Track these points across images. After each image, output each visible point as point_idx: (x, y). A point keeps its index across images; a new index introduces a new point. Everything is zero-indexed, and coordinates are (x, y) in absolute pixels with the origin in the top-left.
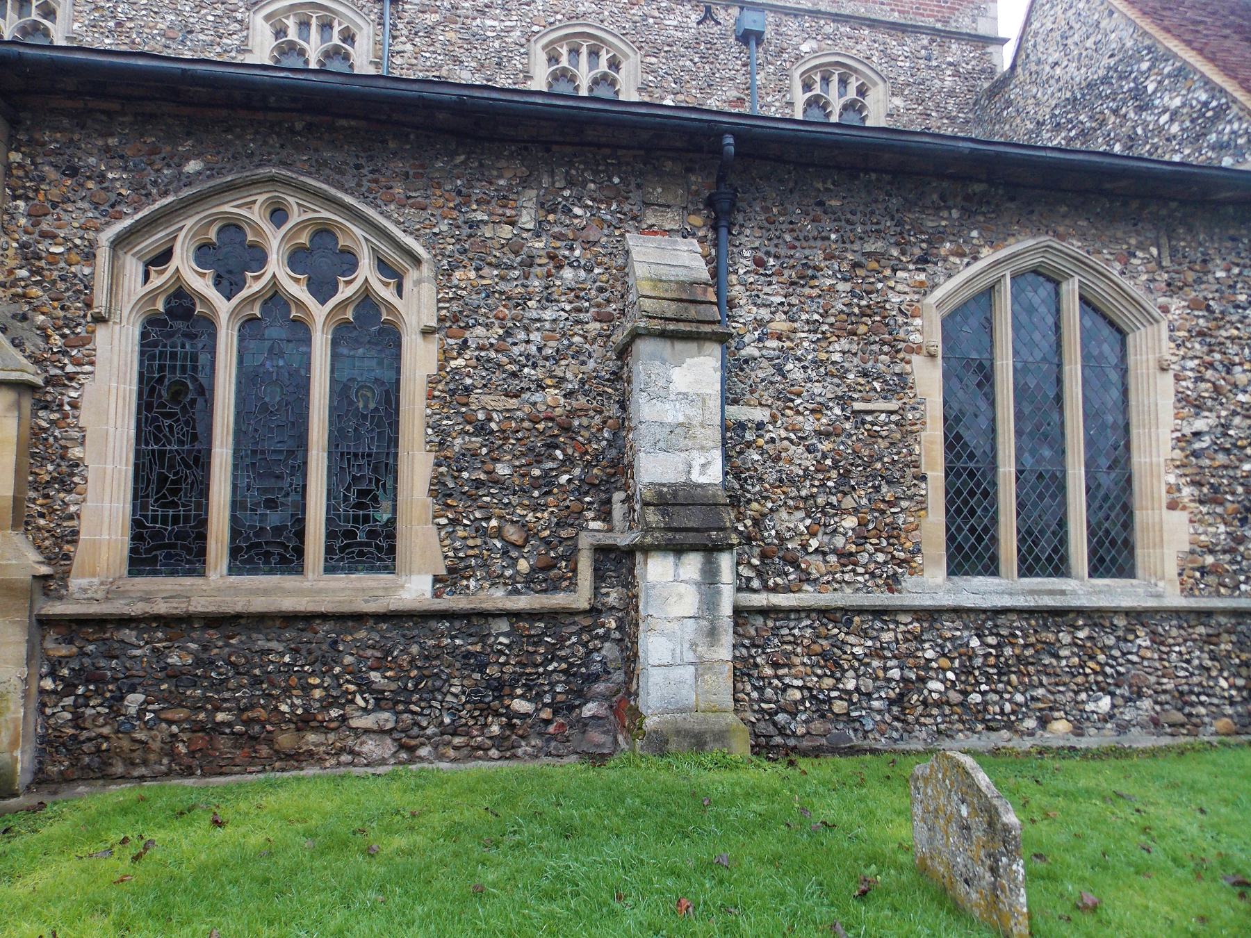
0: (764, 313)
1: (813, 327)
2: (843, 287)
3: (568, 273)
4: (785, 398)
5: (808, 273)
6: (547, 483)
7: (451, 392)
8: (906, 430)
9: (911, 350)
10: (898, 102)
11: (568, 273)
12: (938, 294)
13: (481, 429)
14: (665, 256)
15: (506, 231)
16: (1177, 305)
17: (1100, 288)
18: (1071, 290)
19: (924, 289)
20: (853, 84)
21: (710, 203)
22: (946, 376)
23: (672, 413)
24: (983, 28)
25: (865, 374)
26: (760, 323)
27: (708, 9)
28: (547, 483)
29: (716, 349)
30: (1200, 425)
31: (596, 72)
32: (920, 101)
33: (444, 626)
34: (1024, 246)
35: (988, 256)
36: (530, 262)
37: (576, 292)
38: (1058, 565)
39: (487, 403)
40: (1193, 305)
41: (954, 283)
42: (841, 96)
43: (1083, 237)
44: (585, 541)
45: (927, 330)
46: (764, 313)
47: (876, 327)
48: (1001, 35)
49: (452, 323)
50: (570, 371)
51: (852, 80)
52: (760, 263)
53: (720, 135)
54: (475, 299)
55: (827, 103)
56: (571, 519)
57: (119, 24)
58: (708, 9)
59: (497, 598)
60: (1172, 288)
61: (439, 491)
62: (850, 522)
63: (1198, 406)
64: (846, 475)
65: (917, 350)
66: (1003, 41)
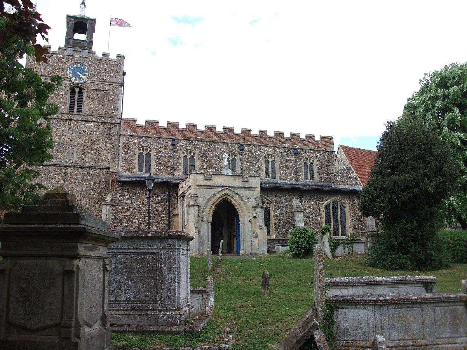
0: (306, 207)
1: (311, 209)
2: (314, 204)
3: (286, 204)
4: (308, 217)
5: (310, 202)
6: (285, 226)
7: (276, 217)
8: (321, 220)
9: (321, 211)
10: (318, 163)
11: (286, 204)
12: (324, 204)
13: (279, 220)
14: (296, 202)
15: (280, 199)
16: (350, 204)
17: (342, 203)
18: (339, 203)
19: (323, 204)
20: (311, 160)
21: (300, 195)
22: (325, 213)
23: (299, 219)
24: (332, 150)
25: (316, 214)
26: (305, 208)
27: (289, 150)
28: (285, 226)
29: (303, 213)
30: (353, 218)
31: (272, 160)
32: (322, 162)
33: (276, 241)
34: (333, 198)
35: (329, 200)
36: (282, 203)
37: (287, 206)
38: (338, 235)
39: (279, 217)
40: (352, 204)
41: (325, 203)
42: (309, 161)
43: (340, 197)
44: (289, 232)
45: (323, 209)
46: (306, 207)
47: (318, 208)
48: (334, 150)
49: (275, 210)
50: (287, 214)
51: (311, 159)
52: (305, 202)
53: (302, 190)
54: (277, 207)
55: (307, 163)
56: (287, 230)
57: (205, 156)
58: (289, 150)
59: (281, 238)
60: (350, 203)
61: (275, 227)
62: (315, 230)
63: (353, 216)
64: (315, 225)
65: (322, 211)
66: (335, 151)
